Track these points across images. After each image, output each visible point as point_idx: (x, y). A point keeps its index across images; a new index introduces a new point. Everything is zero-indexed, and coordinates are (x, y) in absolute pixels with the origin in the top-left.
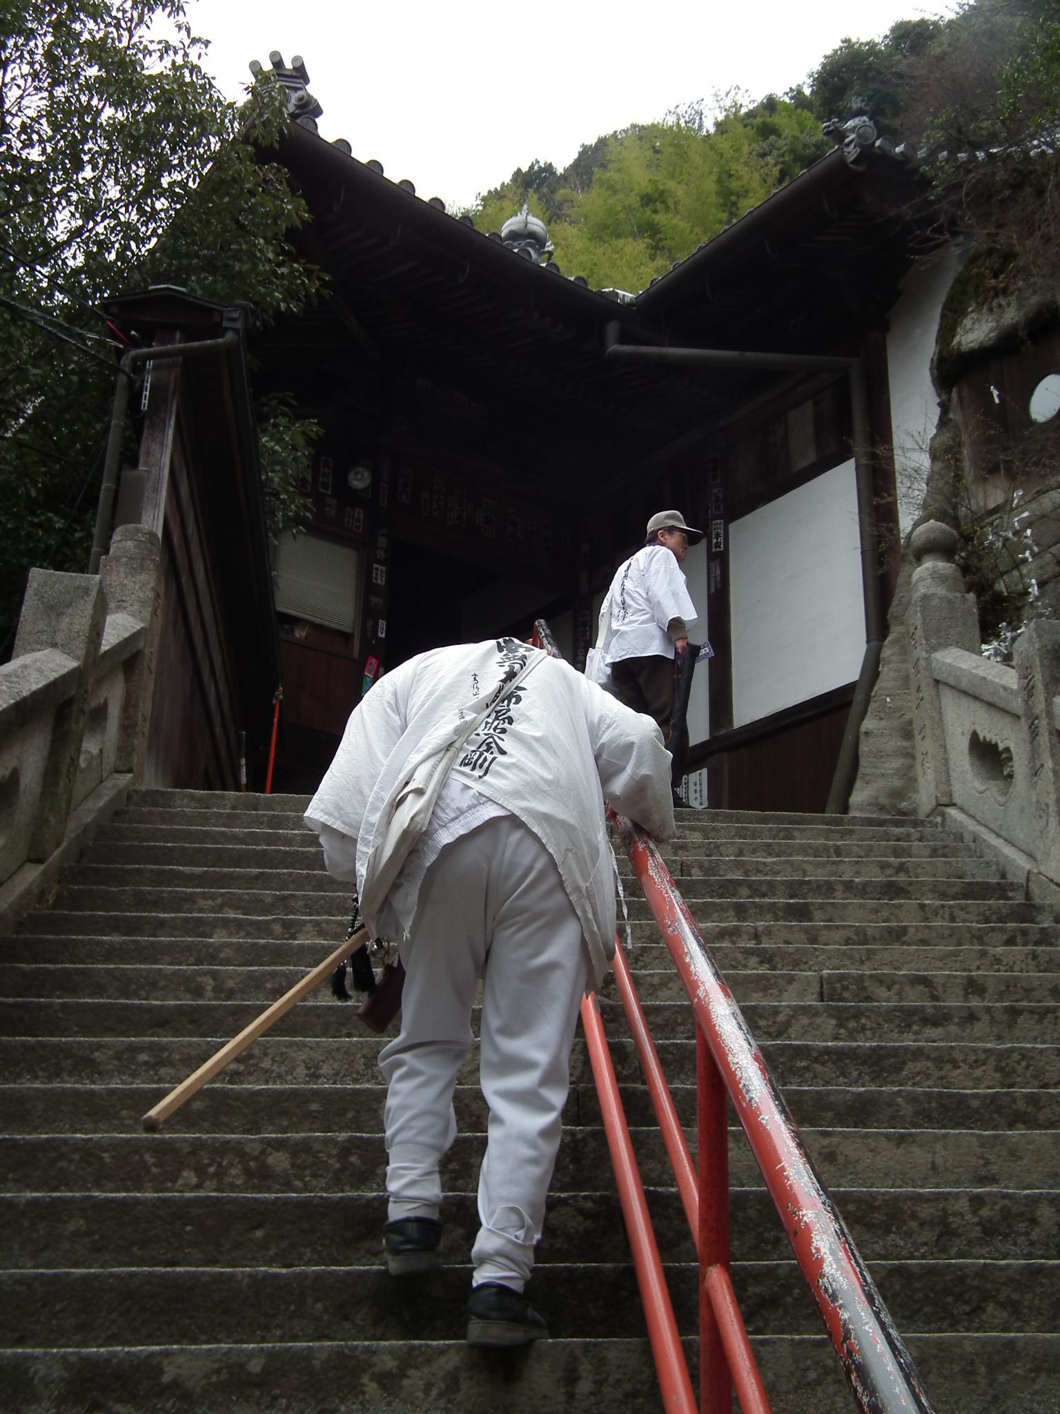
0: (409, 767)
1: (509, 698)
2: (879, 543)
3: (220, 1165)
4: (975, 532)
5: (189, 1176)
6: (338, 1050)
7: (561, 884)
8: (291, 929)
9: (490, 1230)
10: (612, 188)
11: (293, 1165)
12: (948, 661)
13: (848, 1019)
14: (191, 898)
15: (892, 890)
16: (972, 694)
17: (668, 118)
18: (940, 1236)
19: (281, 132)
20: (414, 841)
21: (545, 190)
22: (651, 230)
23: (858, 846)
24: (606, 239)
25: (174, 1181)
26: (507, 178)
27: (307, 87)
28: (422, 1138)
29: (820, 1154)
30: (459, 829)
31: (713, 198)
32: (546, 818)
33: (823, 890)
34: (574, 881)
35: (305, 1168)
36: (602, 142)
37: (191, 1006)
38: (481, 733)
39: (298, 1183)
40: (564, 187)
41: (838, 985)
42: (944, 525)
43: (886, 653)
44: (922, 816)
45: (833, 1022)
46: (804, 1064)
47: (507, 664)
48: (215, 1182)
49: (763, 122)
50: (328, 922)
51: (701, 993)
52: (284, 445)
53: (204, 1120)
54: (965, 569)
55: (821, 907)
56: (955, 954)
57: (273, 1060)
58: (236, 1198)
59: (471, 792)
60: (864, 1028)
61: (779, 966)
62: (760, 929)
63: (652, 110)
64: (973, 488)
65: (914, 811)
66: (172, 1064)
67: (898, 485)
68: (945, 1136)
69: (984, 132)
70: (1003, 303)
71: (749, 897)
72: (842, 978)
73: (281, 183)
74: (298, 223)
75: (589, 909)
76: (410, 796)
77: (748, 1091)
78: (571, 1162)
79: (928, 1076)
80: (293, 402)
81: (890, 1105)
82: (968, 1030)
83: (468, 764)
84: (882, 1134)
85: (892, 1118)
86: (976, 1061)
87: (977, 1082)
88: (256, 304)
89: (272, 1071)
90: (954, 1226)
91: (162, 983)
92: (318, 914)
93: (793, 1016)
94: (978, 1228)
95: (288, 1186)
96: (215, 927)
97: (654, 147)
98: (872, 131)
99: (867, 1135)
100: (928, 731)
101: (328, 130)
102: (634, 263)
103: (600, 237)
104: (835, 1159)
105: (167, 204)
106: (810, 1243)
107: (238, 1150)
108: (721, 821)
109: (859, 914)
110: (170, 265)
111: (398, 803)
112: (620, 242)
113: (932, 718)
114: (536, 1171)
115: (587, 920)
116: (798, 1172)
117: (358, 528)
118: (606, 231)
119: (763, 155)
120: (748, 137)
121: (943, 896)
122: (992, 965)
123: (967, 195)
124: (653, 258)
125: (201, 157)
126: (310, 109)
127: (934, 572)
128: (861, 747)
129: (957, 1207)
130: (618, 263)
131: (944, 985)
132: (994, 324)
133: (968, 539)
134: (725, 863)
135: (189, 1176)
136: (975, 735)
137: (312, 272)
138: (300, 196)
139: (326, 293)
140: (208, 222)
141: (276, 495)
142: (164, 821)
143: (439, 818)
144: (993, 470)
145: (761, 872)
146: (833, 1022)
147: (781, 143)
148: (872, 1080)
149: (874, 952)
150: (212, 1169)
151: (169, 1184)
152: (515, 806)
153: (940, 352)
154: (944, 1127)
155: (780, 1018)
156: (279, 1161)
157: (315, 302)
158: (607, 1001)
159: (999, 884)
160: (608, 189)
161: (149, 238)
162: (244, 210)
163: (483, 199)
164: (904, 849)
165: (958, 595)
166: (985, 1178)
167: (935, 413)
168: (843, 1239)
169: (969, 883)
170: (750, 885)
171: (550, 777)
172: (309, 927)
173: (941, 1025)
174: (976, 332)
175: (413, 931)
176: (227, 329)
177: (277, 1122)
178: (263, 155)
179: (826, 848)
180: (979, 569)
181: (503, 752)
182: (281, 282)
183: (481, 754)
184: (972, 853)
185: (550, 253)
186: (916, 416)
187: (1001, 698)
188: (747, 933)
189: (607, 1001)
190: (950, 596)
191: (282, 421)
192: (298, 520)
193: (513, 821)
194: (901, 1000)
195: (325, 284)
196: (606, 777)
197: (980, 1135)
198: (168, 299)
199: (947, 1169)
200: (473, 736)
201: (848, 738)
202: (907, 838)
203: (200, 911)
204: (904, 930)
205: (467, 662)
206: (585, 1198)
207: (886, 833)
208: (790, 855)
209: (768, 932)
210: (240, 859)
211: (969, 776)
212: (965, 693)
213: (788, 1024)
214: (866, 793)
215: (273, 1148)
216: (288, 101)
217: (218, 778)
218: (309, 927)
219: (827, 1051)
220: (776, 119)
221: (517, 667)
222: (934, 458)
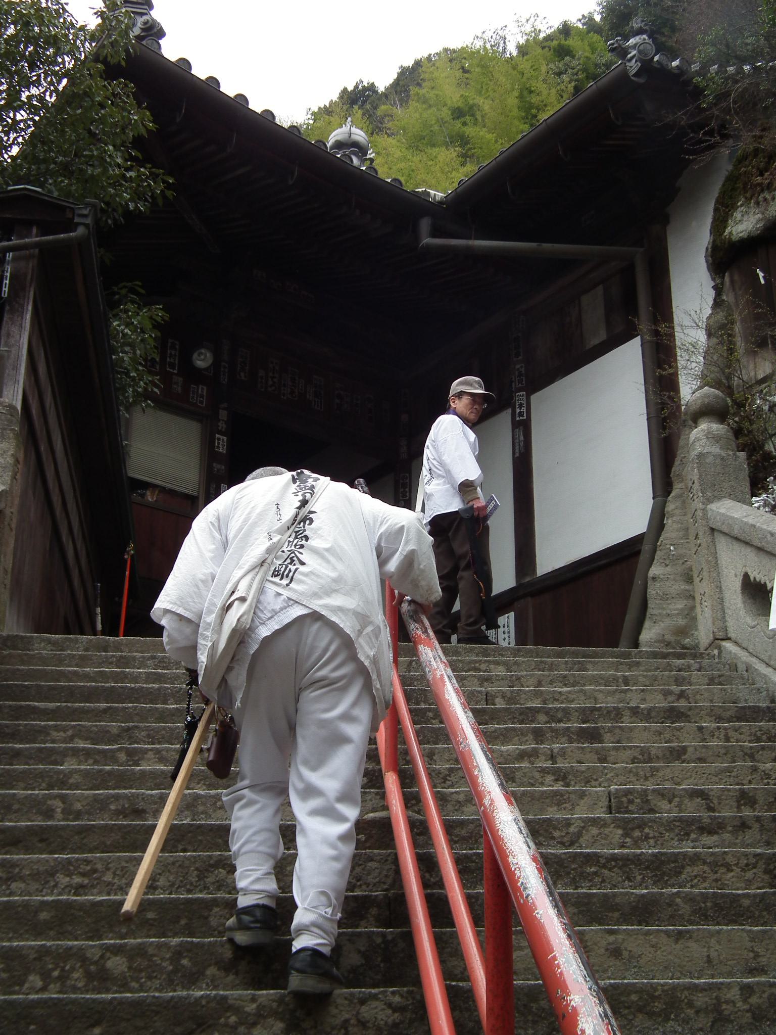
2: (663, 409)
3: (63, 970)
4: (747, 399)
5: (35, 980)
6: (173, 863)
8: (134, 756)
9: (306, 909)
11: (130, 968)
12: (722, 511)
13: (633, 829)
14: (44, 731)
15: (674, 715)
16: (743, 539)
17: (476, 41)
18: (714, 1023)
19: (127, 51)
20: (240, 636)
21: (368, 106)
22: (463, 140)
23: (644, 676)
24: (422, 148)
25: (21, 984)
26: (335, 97)
27: (151, 12)
29: (607, 950)
31: (515, 112)
33: (613, 715)
35: (141, 971)
36: (418, 63)
37: (41, 826)
39: (134, 985)
41: (624, 799)
42: (717, 391)
43: (670, 507)
44: (702, 650)
45: (620, 832)
46: (593, 869)
47: (300, 494)
48: (58, 985)
49: (559, 45)
50: (168, 750)
51: (486, 802)
52: (132, 329)
53: (51, 929)
54: (738, 432)
55: (611, 730)
56: (729, 770)
57: (114, 874)
58: (76, 999)
59: (282, 597)
60: (647, 837)
61: (573, 783)
62: (555, 751)
63: (461, 36)
64: (744, 360)
65: (697, 646)
66: (22, 879)
67: (679, 358)
68: (718, 932)
69: (749, 47)
70: (768, 197)
71: (546, 723)
72: (628, 792)
73: (128, 96)
74: (143, 132)
76: (236, 602)
77: (525, 888)
78: (381, 961)
79: (705, 879)
81: (669, 905)
82: (740, 837)
83: (277, 575)
84: (662, 931)
85: (672, 916)
86: (747, 865)
87: (749, 884)
88: (107, 204)
89: (113, 884)
90: (726, 1013)
91: (16, 807)
92: (159, 743)
93: (583, 827)
94: (749, 1015)
95: (124, 986)
96: (65, 756)
97: (463, 68)
98: (650, 48)
99: (648, 933)
100: (705, 574)
101: (171, 49)
103: (417, 148)
104: (621, 955)
105: (25, 115)
106: (576, 1025)
107: (80, 956)
109: (643, 736)
110: (29, 169)
111: (227, 608)
112: (434, 151)
113: (708, 562)
114: (338, 866)
116: (567, 961)
117: (201, 402)
118: (421, 141)
119: (559, 74)
120: (545, 59)
121: (719, 719)
122: (762, 779)
123: (735, 102)
124: (463, 165)
125: (55, 74)
126: (154, 32)
127: (709, 433)
128: (648, 591)
129: (728, 996)
130: (432, 169)
131: (719, 798)
132: (760, 216)
133: (740, 405)
134: (525, 693)
135: (35, 980)
136: (746, 576)
137: (157, 176)
138: (146, 108)
139: (169, 193)
140: (63, 131)
141: (127, 373)
142: (23, 663)
143: (259, 618)
144: (762, 344)
145: (557, 700)
146: (620, 832)
147: (575, 63)
148: (654, 884)
149: (657, 770)
150: (56, 973)
151: (17, 988)
153: (714, 241)
154: (718, 924)
155: (572, 829)
156: (117, 964)
157: (160, 202)
158: (417, 817)
159: (768, 708)
160: (424, 103)
161: (11, 146)
162: (95, 120)
163: (314, 114)
164: (684, 679)
165: (731, 453)
166: (755, 969)
167: (710, 296)
168: (606, 1021)
169: (743, 708)
170: (547, 712)
172: (150, 755)
173: (716, 833)
174: (745, 224)
176: (78, 224)
177: (117, 930)
178: (112, 72)
179: (615, 679)
180: (750, 432)
181: (303, 563)
182: (131, 186)
183: (287, 567)
184: (744, 681)
185: (372, 160)
186: (694, 297)
187: (768, 543)
188: (544, 754)
189: (417, 817)
190: (723, 453)
191: (130, 306)
192: (147, 395)
193: (315, 616)
194: (680, 811)
195: (169, 186)
197: (750, 931)
198: (26, 198)
199: (721, 962)
200: (280, 553)
201: (638, 582)
202: (688, 668)
203: (53, 742)
204: (684, 750)
206: (393, 993)
207: (669, 665)
208: (584, 685)
209: (563, 753)
210: (90, 695)
211: (742, 613)
212: (737, 539)
213: (579, 835)
214: (653, 631)
215: (112, 952)
216: (134, 25)
217: (76, 624)
218: (150, 755)
219: (614, 858)
220: (570, 42)
222: (709, 335)
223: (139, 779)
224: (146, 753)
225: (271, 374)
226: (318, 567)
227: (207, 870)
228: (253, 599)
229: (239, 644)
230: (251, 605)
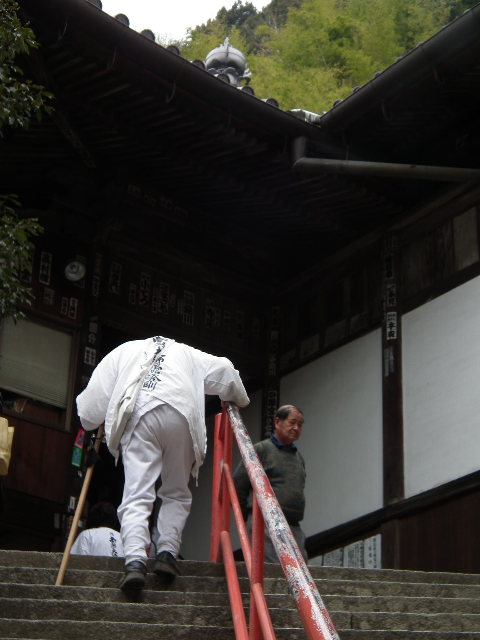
10: (303, 23)
21: (245, 26)
24: (299, 68)
26: (213, 16)
30: (146, 409)
31: (393, 34)
40: (261, 24)
73: (12, 15)
74: (26, 49)
76: (126, 400)
80: (18, 203)
102: (324, 89)
108: (389, 580)
111: (121, 404)
112: (312, 71)
117: (72, 315)
118: (297, 61)
130: (310, 88)
134: (391, 617)
137: (37, 91)
138: (29, 26)
139: (48, 109)
145: (423, 626)
157: (39, 117)
181: (159, 380)
185: (248, 79)
192: (19, 307)
195: (48, 102)
200: (147, 376)
208: (451, 611)
221: (161, 348)
225: (142, 288)
230: (133, 401)
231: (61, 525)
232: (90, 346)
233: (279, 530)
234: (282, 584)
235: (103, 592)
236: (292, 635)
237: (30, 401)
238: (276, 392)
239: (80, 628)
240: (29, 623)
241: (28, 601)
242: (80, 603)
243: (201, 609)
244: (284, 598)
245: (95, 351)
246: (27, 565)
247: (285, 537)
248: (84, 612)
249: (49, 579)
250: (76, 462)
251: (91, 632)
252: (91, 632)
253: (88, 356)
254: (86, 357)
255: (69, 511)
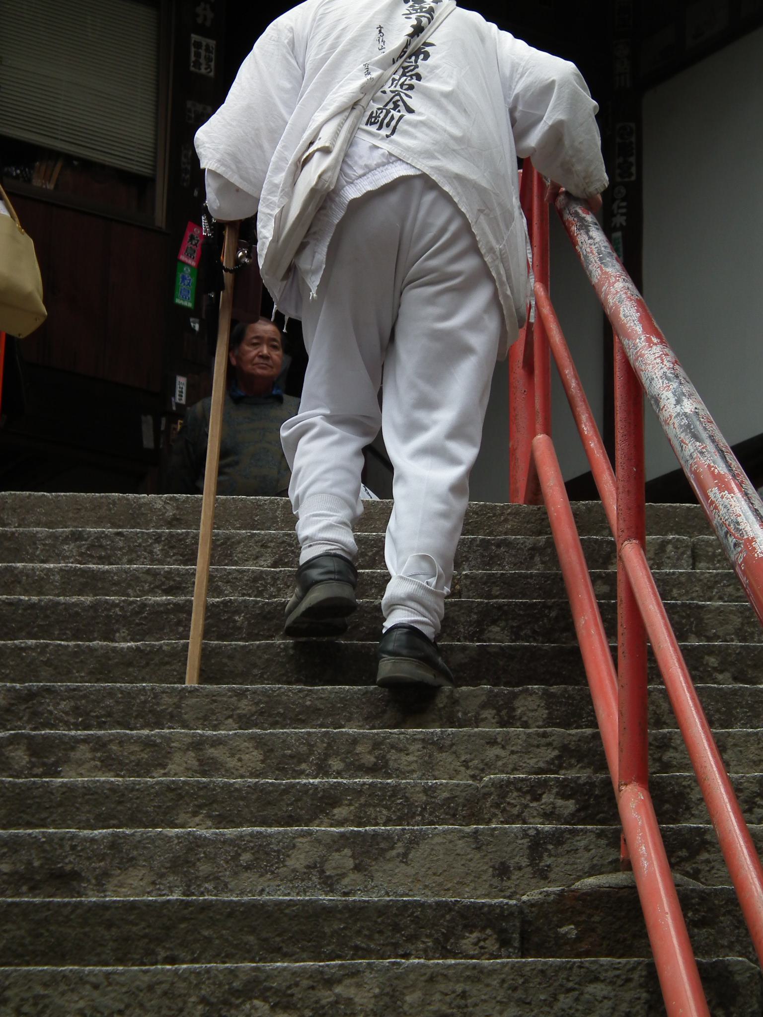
0: (313, 126)
1: (416, 53)
6: (151, 988)
7: (474, 249)
9: (401, 577)
20: (322, 198)
28: (336, 490)
32: (459, 179)
34: (488, 242)
38: (388, 90)
47: (414, 16)
50: (122, 741)
59: (380, 151)
75: (502, 272)
76: (317, 155)
83: (374, 123)
92: (101, 726)
111: (303, 163)
114: (447, 524)
115: (502, 284)
143: (346, 175)
152: (425, 166)
158: (693, 884)
171: (457, 132)
172: (83, 752)
175: (321, 288)
181: (410, 110)
183: (388, 112)
189: (693, 884)
193: (426, 182)
196: (519, 130)
200: (379, 94)
205: (371, 12)
218: (83, 752)
223: (60, 804)
224: (73, 749)
226: (433, 117)
227: (226, 1002)
228: (340, 151)
229: (319, 211)
230: (336, 160)
231: (157, 441)
232: (202, 31)
233: (685, 414)
234: (676, 548)
235: (275, 578)
236: (707, 657)
237: (68, 159)
238: (633, 125)
239: (231, 657)
240: (114, 649)
241: (106, 602)
242: (225, 603)
243: (500, 607)
244: (683, 579)
245: (212, 43)
246: (98, 523)
247: (700, 428)
248: (235, 621)
249: (151, 552)
250: (184, 298)
251: (255, 665)
252: (255, 665)
253: (198, 55)
254: (193, 58)
255: (174, 408)
